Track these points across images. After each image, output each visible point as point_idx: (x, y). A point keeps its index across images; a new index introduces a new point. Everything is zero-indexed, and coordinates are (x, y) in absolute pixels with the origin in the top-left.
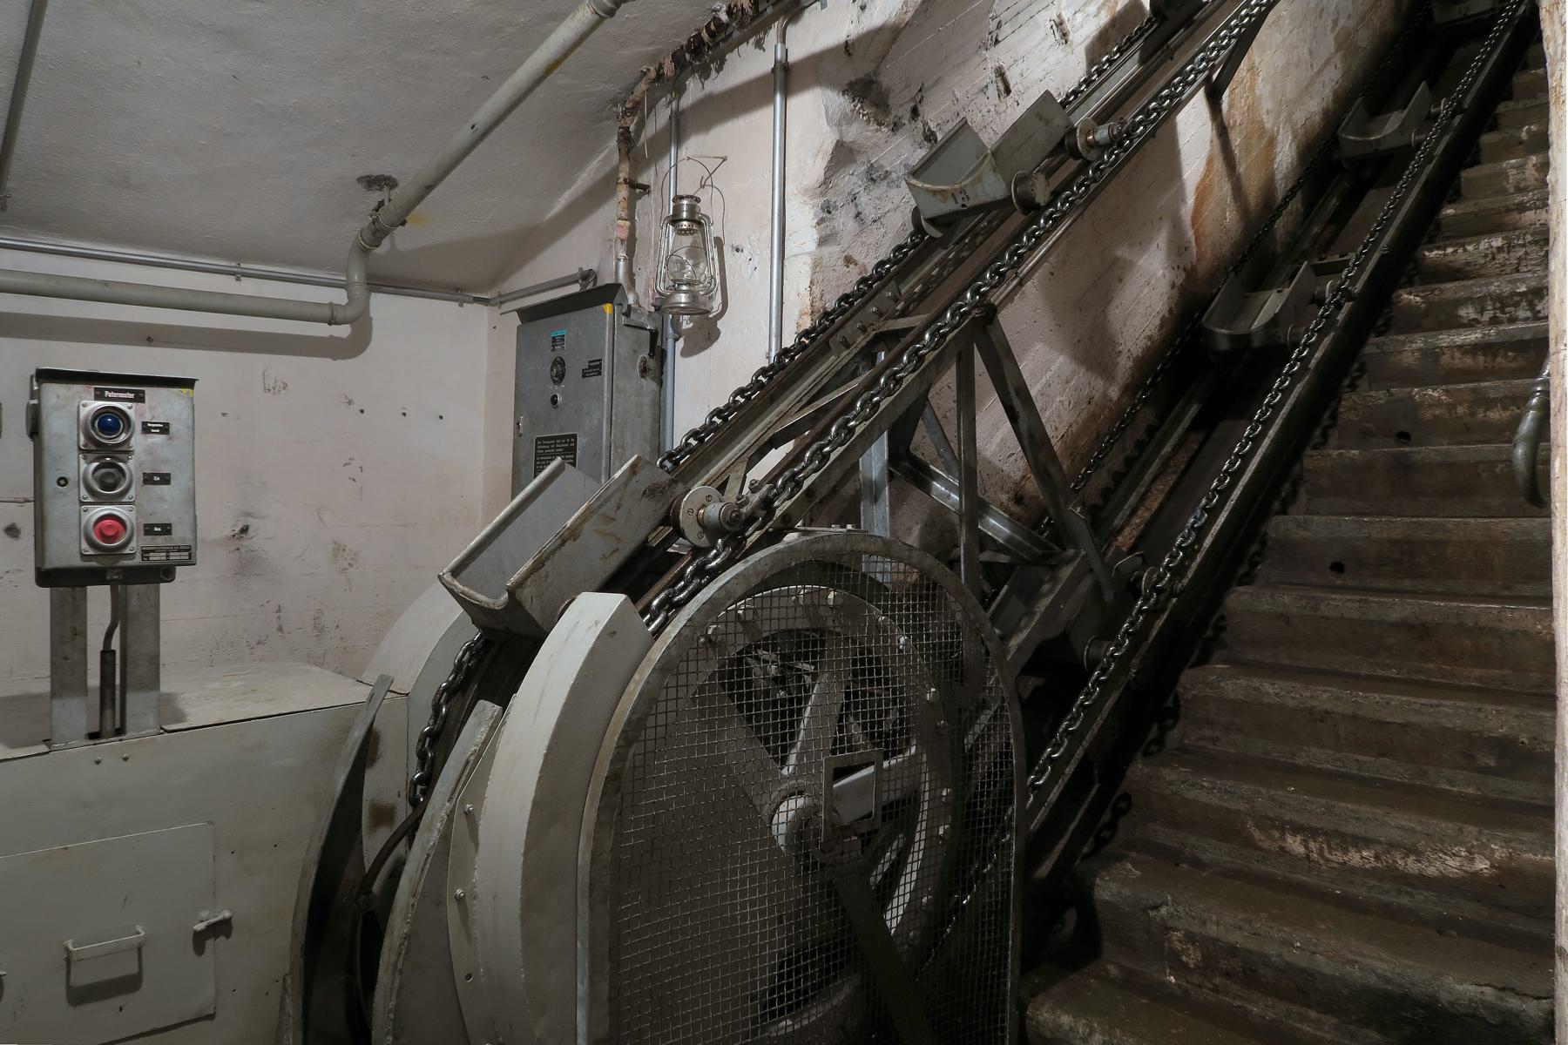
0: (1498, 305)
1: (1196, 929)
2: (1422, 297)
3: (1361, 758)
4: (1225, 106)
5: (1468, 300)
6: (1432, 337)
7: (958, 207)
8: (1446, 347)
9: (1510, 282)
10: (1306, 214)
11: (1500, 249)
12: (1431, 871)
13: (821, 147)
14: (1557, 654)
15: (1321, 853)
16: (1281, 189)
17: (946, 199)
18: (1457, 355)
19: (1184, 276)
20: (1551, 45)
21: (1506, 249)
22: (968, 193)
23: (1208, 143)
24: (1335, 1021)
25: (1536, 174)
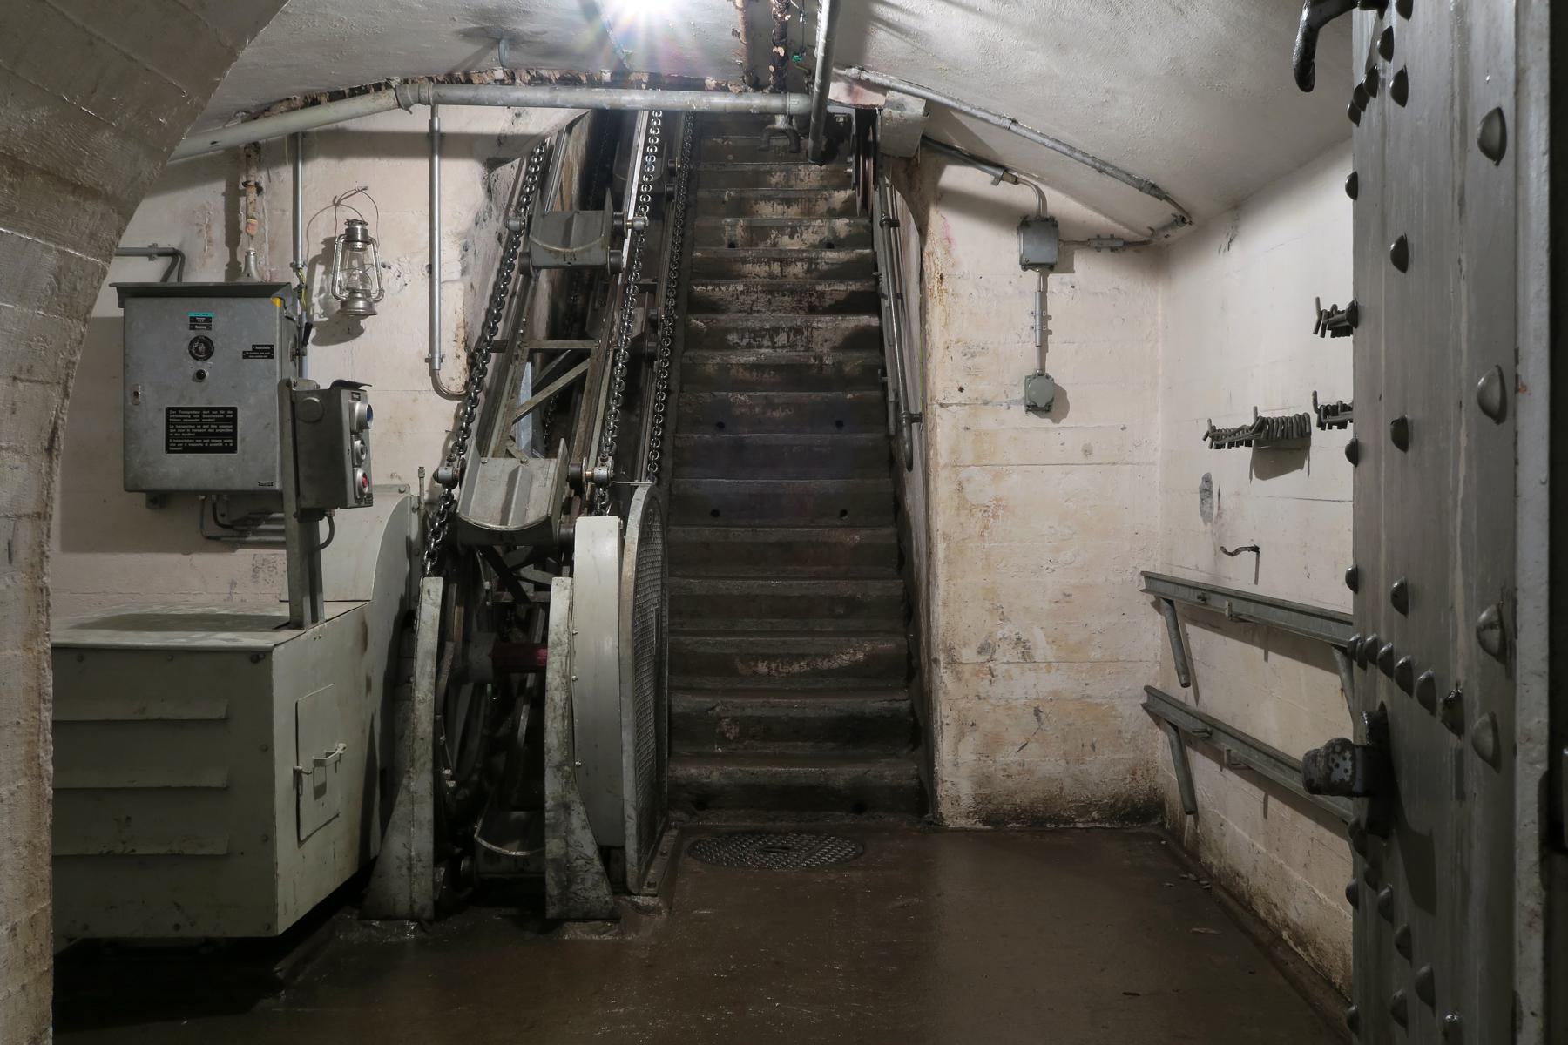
0: (752, 335)
1: (738, 713)
3: (774, 621)
5: (735, 330)
6: (727, 356)
11: (742, 292)
12: (835, 665)
15: (777, 670)
18: (741, 370)
20: (929, 269)
24: (811, 743)
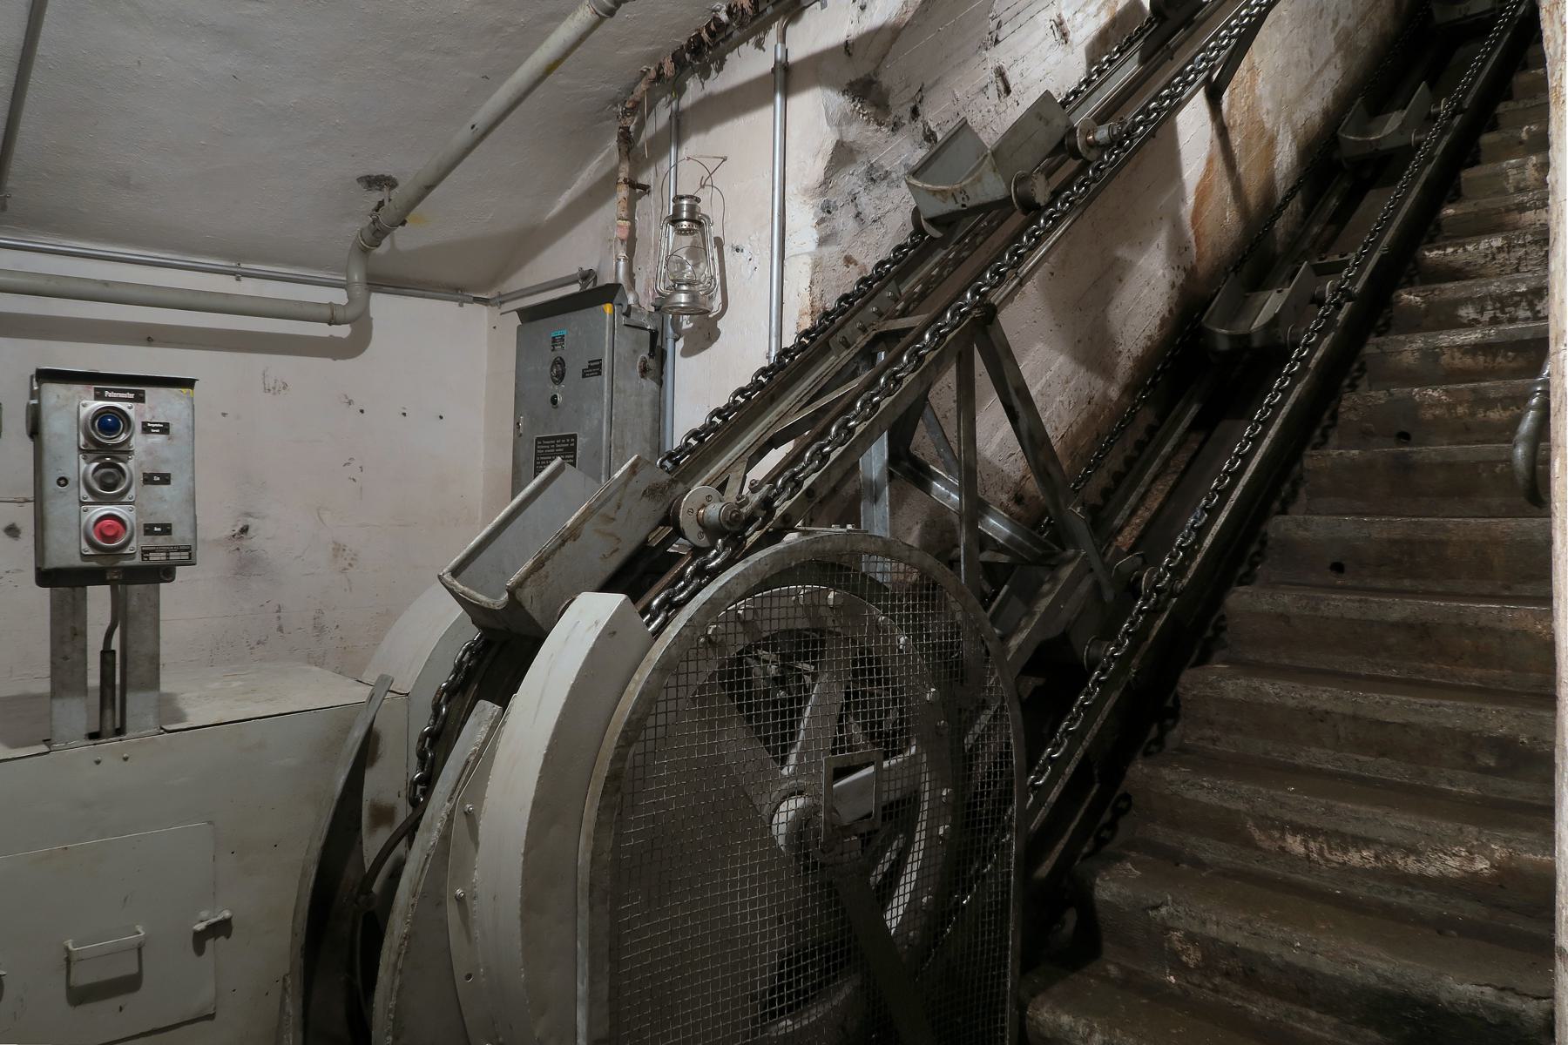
0: (1498, 305)
1: (1196, 929)
2: (1422, 297)
3: (1361, 758)
4: (1225, 106)
5: (1468, 300)
6: (1432, 337)
7: (958, 207)
8: (1446, 347)
9: (1510, 282)
10: (1306, 214)
11: (1500, 249)
12: (1431, 871)
13: (821, 147)
14: (1557, 654)
15: (1321, 853)
16: (1281, 189)
17: (946, 199)
18: (1457, 355)
19: (1184, 276)
20: (1551, 45)
21: (1506, 249)
22: (968, 193)
23: (1208, 143)
24: (1335, 1021)
25: (1536, 174)
